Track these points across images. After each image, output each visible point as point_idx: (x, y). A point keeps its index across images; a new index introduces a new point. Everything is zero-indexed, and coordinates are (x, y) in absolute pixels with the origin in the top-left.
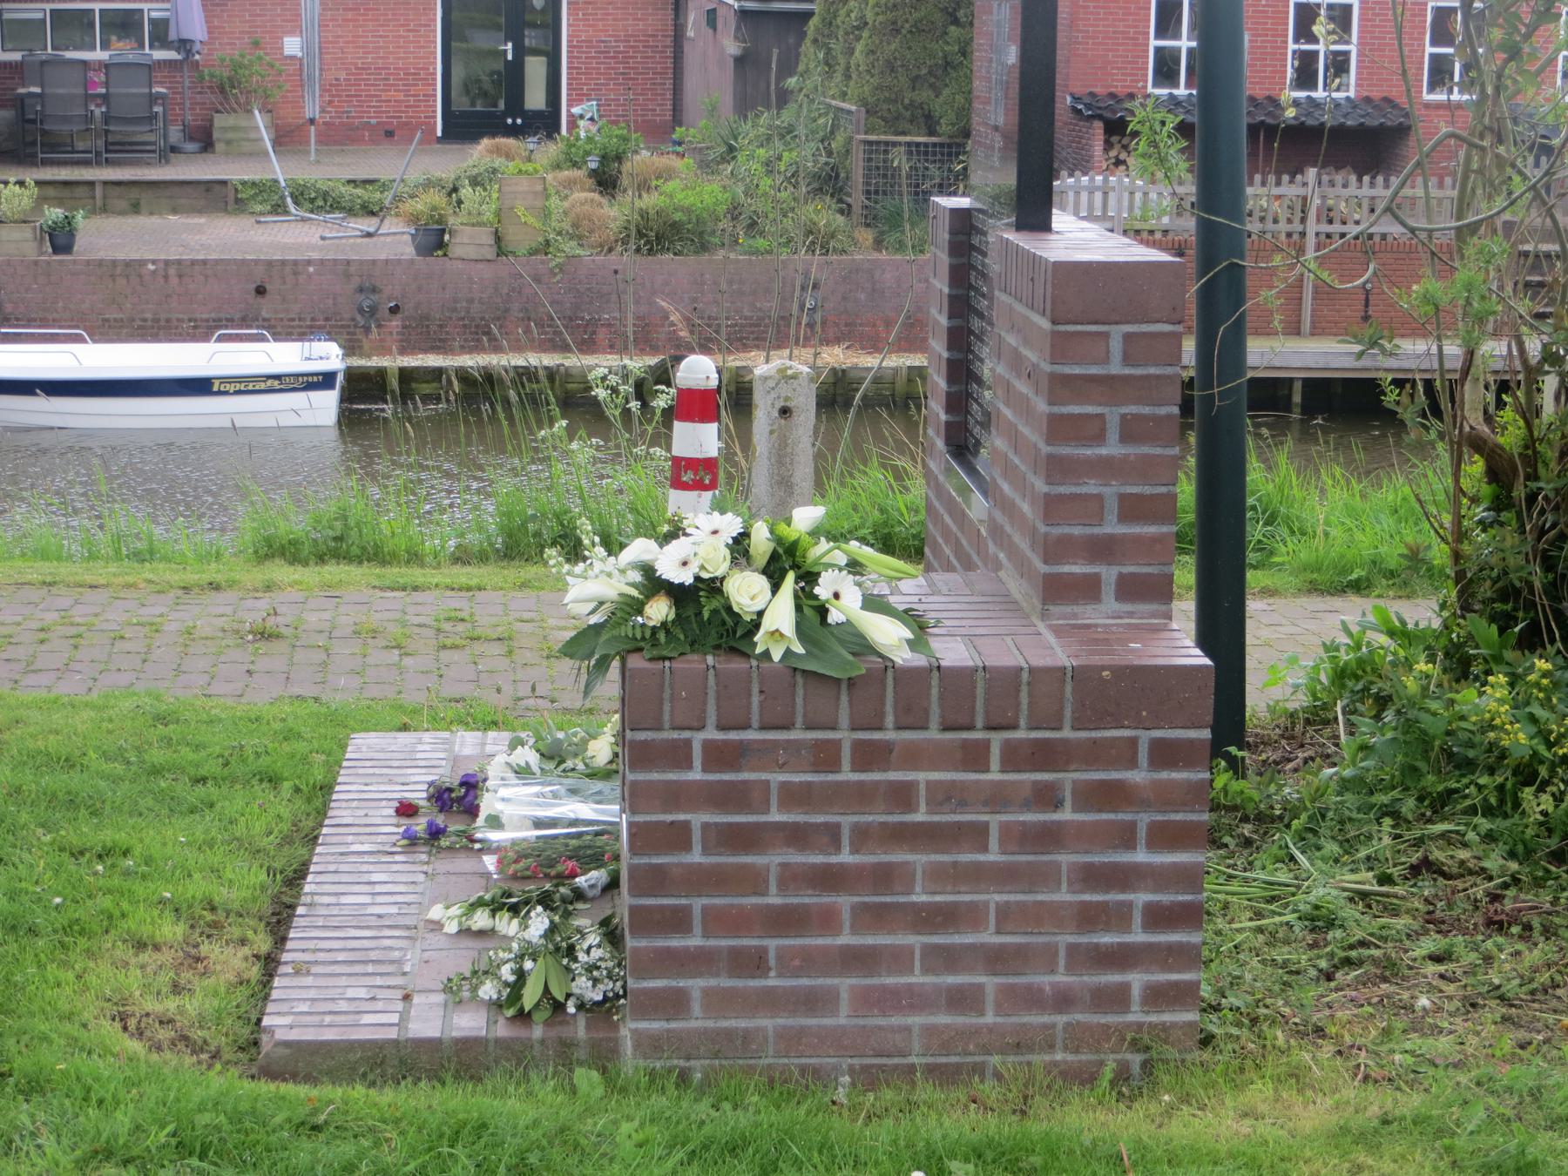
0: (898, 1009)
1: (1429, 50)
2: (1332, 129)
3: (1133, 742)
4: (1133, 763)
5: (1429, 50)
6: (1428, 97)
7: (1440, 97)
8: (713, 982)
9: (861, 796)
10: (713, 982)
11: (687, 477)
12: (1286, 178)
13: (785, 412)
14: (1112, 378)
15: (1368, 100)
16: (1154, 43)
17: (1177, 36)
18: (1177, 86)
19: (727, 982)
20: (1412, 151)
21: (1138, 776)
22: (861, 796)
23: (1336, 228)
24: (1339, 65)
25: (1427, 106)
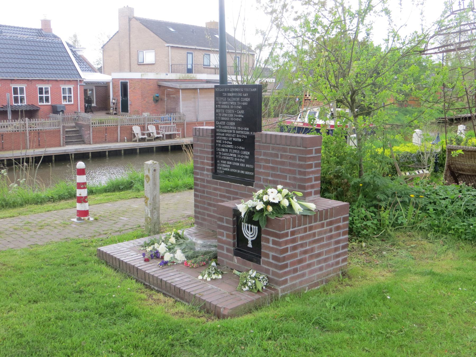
0: (314, 273)
1: (39, 95)
2: (25, 111)
3: (340, 218)
4: (340, 222)
5: (39, 95)
6: (40, 104)
7: (42, 104)
8: (291, 276)
9: (308, 236)
10: (291, 276)
11: (82, 187)
12: (13, 120)
13: (155, 170)
14: (314, 157)
15: (29, 105)
16: (62, 95)
17: (18, 94)
18: (18, 103)
19: (293, 275)
20: (40, 113)
21: (341, 224)
22: (308, 236)
23: (32, 129)
24: (22, 99)
25: (40, 105)
